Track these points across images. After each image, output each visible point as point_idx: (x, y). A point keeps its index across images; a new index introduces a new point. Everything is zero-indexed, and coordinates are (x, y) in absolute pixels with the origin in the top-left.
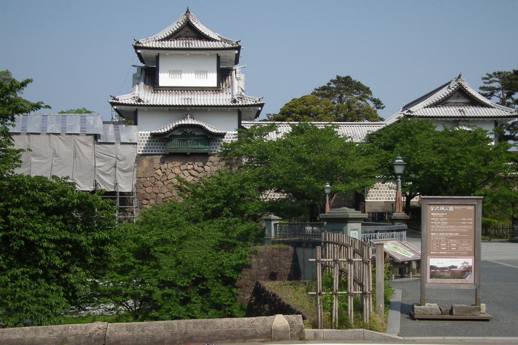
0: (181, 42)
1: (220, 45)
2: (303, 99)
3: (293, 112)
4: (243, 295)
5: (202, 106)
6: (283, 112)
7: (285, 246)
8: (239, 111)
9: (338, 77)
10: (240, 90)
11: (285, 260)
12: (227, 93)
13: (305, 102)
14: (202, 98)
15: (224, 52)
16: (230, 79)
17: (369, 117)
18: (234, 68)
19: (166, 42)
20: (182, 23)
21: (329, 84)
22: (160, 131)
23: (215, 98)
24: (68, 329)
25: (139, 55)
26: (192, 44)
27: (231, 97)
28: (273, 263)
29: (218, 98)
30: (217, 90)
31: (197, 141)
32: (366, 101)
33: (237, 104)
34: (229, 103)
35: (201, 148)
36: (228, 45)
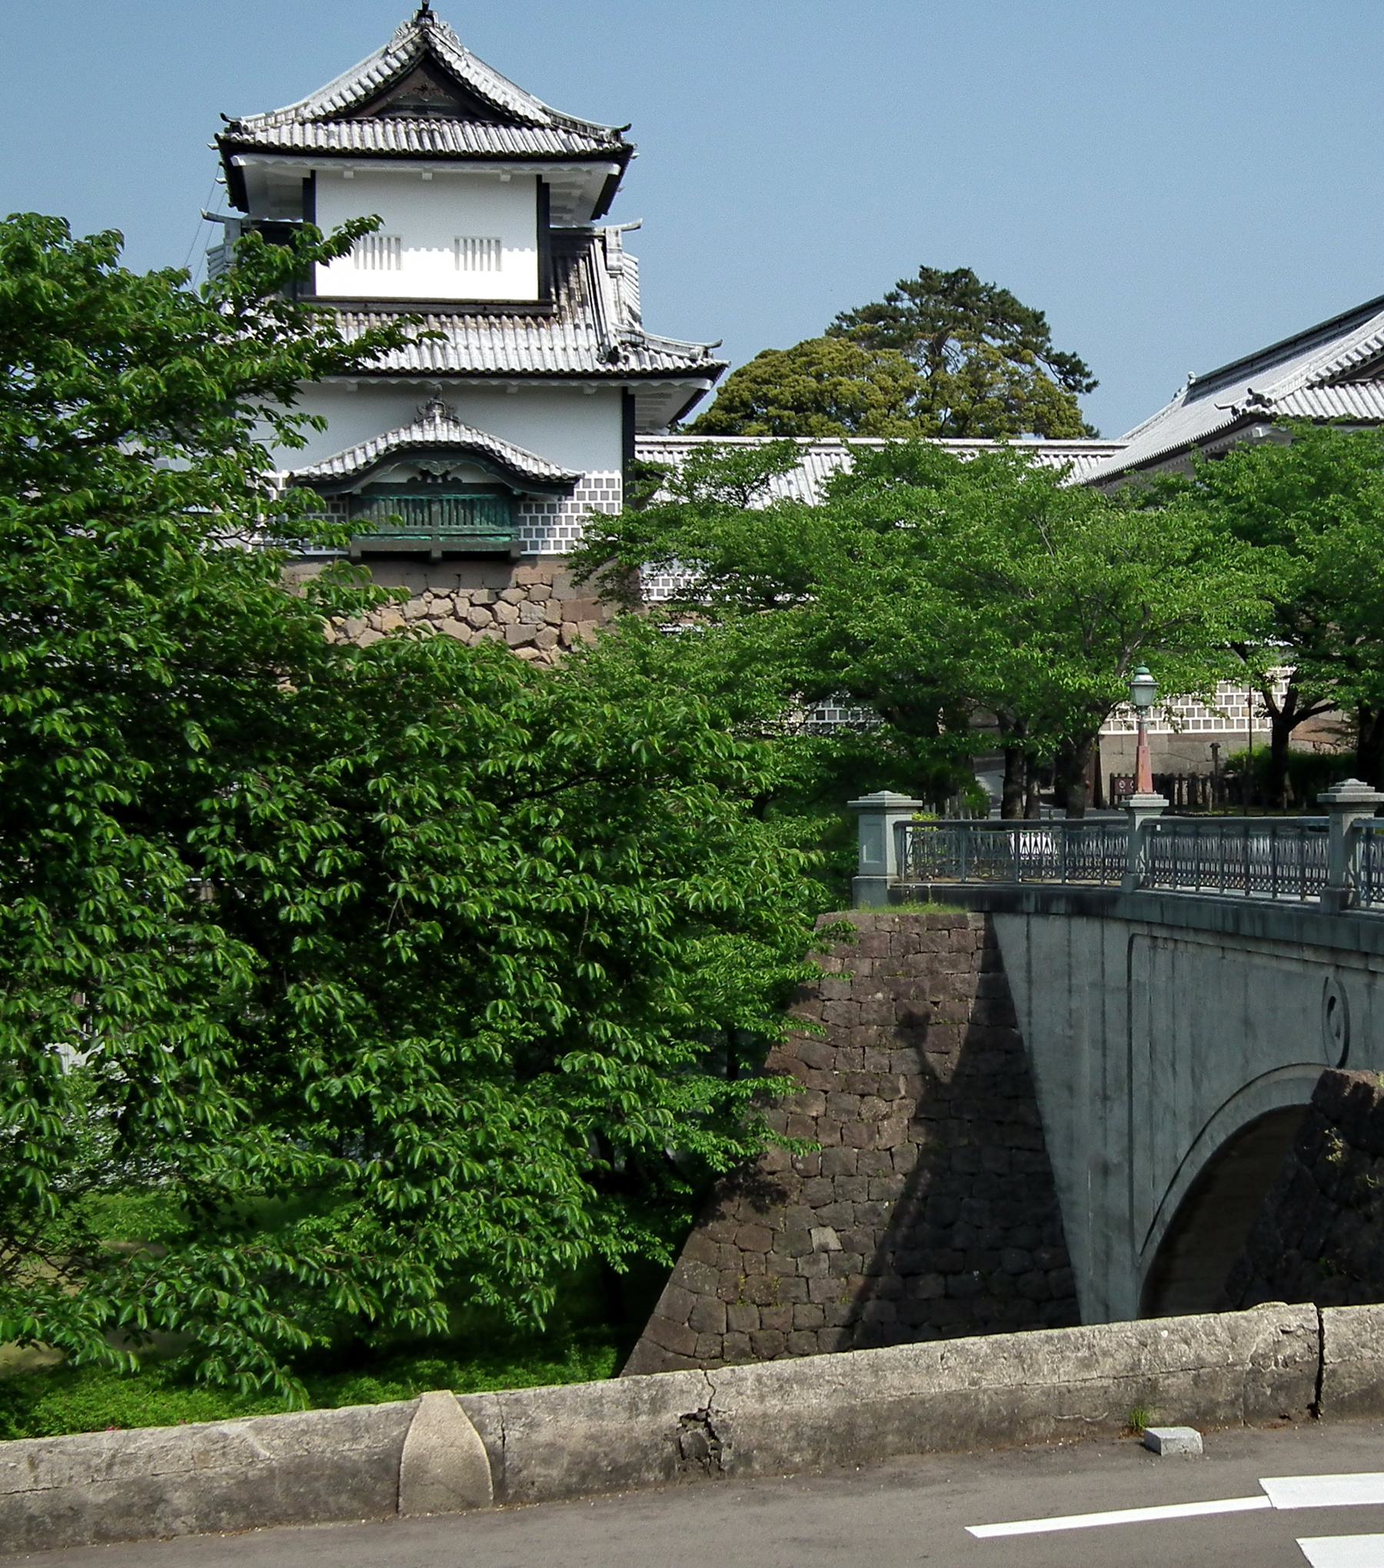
0: (401, 127)
1: (551, 142)
2: (803, 353)
3: (767, 401)
4: (797, 1103)
5: (487, 374)
6: (731, 401)
7: (952, 911)
8: (628, 394)
9: (925, 272)
10: (626, 315)
11: (954, 965)
12: (576, 326)
13: (811, 364)
14: (486, 343)
15: (566, 167)
16: (583, 272)
17: (1051, 423)
18: (598, 231)
19: (344, 127)
20: (404, 56)
21: (891, 298)
22: (326, 470)
23: (546, 344)
24: (1157, 1340)
25: (235, 176)
26: (443, 136)
27: (593, 341)
28: (907, 974)
29: (546, 344)
30: (537, 313)
31: (470, 505)
32: (1032, 364)
33: (621, 365)
34: (590, 363)
35: (485, 532)
36: (580, 144)
